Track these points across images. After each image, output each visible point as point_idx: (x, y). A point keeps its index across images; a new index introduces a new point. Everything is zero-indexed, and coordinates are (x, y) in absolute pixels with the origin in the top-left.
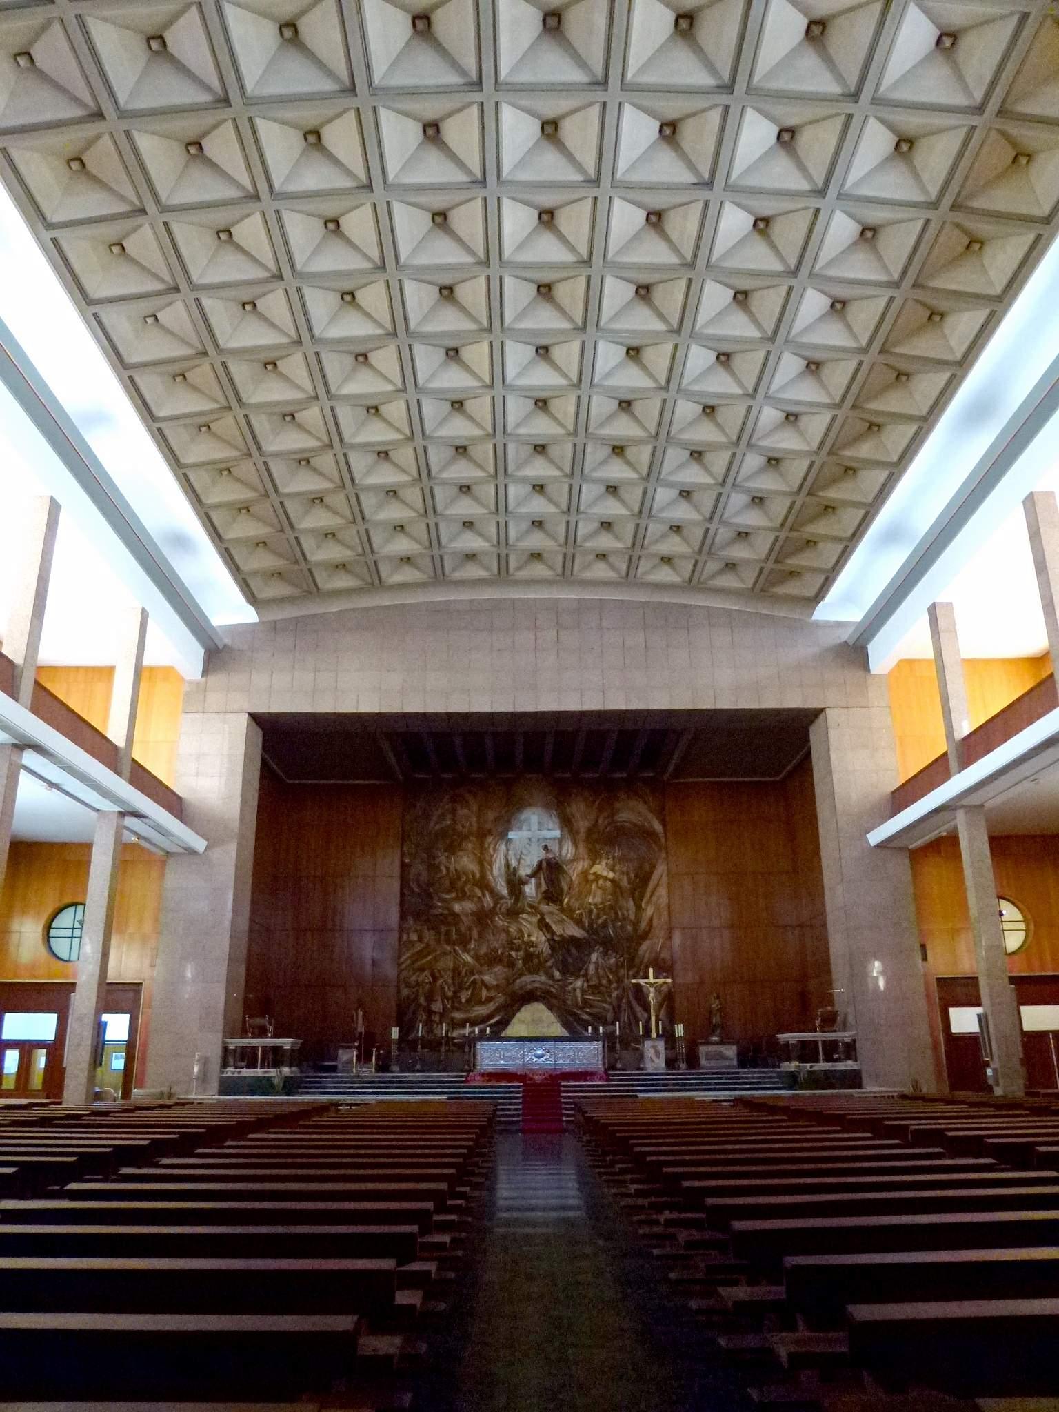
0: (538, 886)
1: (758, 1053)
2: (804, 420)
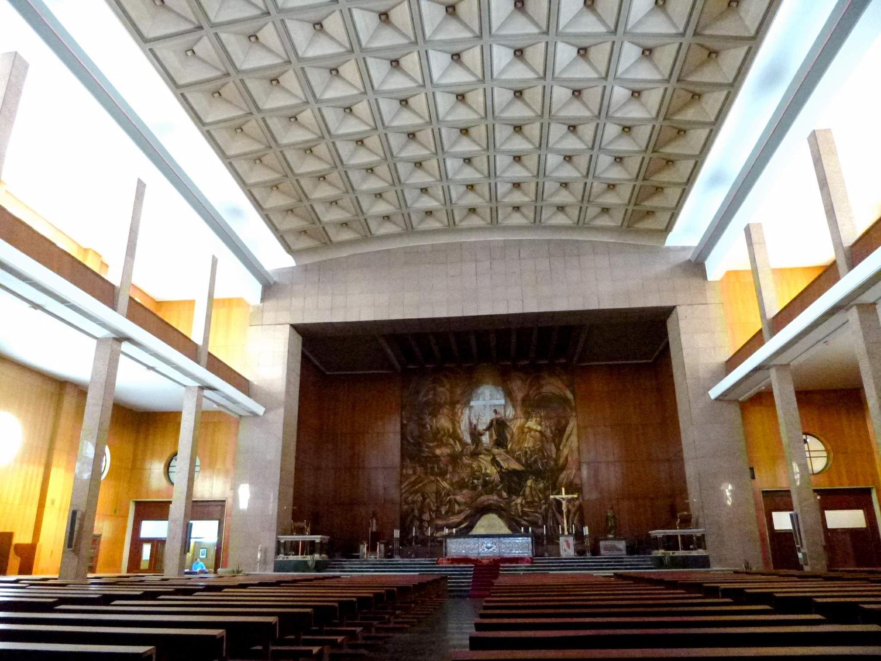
0: (491, 436)
1: (640, 546)
2: (645, 94)
